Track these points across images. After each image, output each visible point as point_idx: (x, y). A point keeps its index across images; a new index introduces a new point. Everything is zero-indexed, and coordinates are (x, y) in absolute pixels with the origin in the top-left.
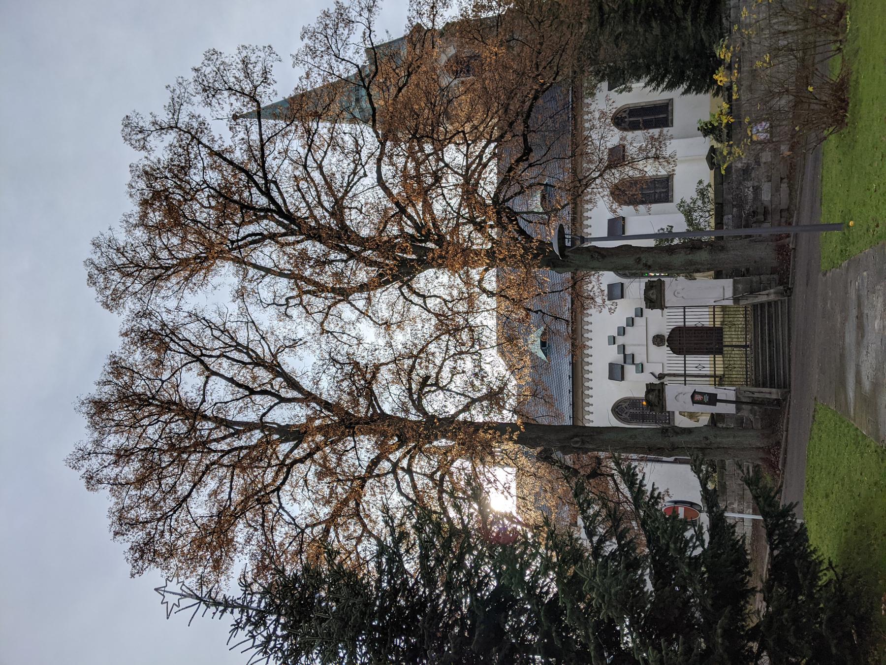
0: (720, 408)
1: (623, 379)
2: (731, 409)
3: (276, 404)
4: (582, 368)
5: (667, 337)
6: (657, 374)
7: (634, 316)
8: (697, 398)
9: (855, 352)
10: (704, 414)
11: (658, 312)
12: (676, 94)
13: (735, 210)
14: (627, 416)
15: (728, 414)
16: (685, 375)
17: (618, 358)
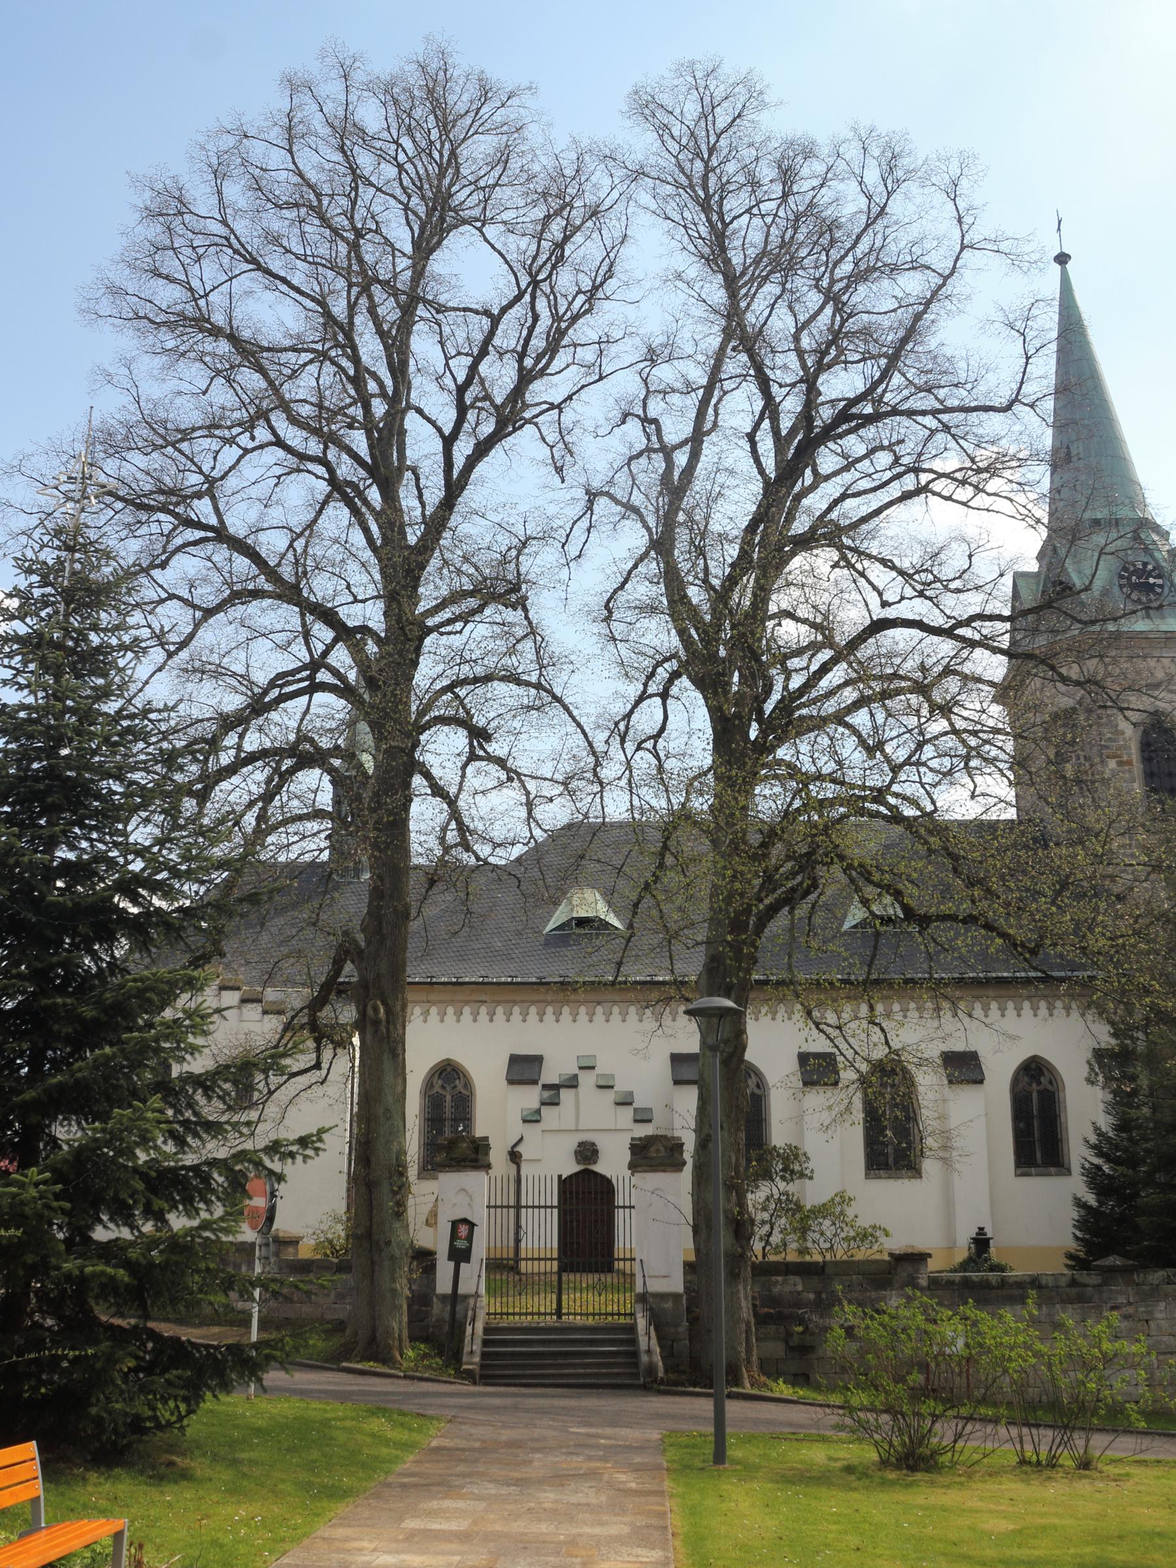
0: (444, 1269)
1: (511, 1082)
2: (443, 1285)
3: (439, 430)
4: (533, 1002)
5: (597, 1168)
6: (519, 1149)
7: (635, 1105)
8: (462, 1227)
9: (504, 1438)
10: (437, 1240)
11: (627, 1156)
12: (1075, 1185)
13: (812, 1296)
14: (437, 1088)
15: (434, 1280)
16: (518, 1207)
17: (550, 1075)
